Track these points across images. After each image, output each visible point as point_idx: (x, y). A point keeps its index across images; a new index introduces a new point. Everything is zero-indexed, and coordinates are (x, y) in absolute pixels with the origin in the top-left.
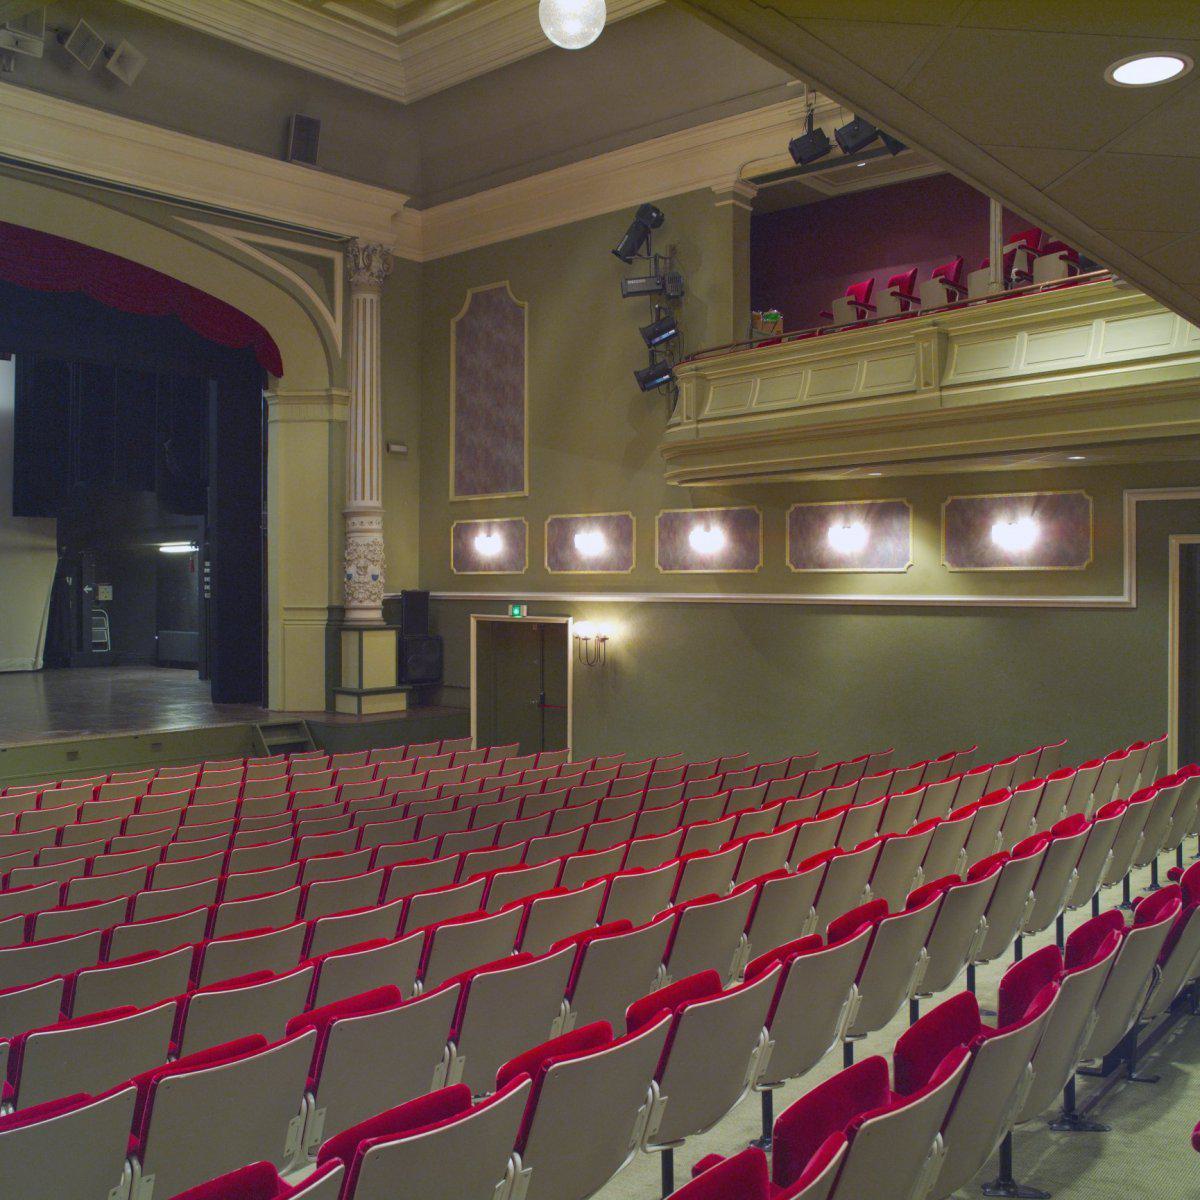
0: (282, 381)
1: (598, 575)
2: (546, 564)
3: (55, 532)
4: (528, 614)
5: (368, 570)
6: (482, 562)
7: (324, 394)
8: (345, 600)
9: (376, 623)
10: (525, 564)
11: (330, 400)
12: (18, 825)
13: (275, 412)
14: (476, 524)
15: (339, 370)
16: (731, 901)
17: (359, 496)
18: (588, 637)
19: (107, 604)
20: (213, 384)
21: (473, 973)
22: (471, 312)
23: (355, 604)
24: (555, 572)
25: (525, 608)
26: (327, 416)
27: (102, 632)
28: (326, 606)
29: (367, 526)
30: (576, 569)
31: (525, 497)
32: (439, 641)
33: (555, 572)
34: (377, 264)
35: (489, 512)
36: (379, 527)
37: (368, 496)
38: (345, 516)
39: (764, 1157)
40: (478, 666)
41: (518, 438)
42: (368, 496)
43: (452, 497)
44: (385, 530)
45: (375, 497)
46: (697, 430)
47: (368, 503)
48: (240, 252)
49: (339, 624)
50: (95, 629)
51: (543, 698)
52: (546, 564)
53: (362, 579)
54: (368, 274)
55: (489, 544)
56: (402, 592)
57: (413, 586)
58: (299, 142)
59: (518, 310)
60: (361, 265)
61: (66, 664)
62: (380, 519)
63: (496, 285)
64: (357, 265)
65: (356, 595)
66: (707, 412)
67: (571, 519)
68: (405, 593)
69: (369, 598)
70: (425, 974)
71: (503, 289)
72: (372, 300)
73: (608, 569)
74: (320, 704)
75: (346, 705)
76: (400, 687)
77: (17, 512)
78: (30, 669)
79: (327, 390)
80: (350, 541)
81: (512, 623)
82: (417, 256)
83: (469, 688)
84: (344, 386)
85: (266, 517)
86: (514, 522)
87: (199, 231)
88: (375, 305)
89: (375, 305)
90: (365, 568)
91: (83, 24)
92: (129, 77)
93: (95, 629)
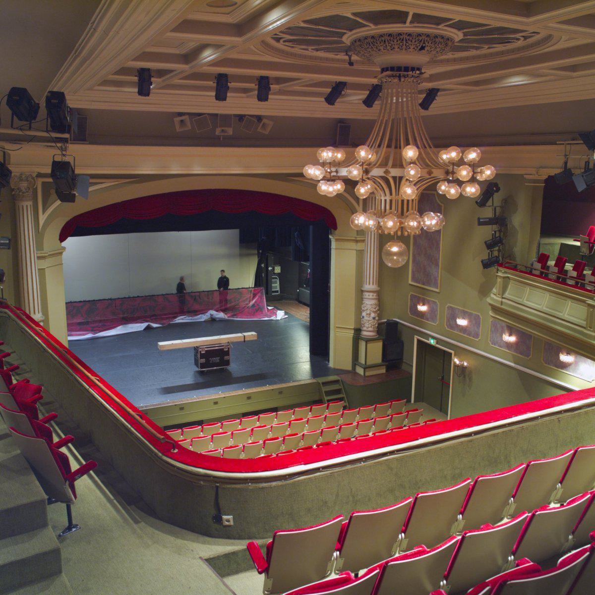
0: (337, 232)
13: (334, 245)
17: (368, 284)
19: (278, 274)
20: (311, 227)
27: (276, 286)
28: (353, 328)
32: (402, 343)
39: (441, 592)
41: (437, 265)
45: (375, 284)
46: (502, 302)
50: (273, 285)
66: (506, 295)
80: (364, 302)
93: (273, 285)
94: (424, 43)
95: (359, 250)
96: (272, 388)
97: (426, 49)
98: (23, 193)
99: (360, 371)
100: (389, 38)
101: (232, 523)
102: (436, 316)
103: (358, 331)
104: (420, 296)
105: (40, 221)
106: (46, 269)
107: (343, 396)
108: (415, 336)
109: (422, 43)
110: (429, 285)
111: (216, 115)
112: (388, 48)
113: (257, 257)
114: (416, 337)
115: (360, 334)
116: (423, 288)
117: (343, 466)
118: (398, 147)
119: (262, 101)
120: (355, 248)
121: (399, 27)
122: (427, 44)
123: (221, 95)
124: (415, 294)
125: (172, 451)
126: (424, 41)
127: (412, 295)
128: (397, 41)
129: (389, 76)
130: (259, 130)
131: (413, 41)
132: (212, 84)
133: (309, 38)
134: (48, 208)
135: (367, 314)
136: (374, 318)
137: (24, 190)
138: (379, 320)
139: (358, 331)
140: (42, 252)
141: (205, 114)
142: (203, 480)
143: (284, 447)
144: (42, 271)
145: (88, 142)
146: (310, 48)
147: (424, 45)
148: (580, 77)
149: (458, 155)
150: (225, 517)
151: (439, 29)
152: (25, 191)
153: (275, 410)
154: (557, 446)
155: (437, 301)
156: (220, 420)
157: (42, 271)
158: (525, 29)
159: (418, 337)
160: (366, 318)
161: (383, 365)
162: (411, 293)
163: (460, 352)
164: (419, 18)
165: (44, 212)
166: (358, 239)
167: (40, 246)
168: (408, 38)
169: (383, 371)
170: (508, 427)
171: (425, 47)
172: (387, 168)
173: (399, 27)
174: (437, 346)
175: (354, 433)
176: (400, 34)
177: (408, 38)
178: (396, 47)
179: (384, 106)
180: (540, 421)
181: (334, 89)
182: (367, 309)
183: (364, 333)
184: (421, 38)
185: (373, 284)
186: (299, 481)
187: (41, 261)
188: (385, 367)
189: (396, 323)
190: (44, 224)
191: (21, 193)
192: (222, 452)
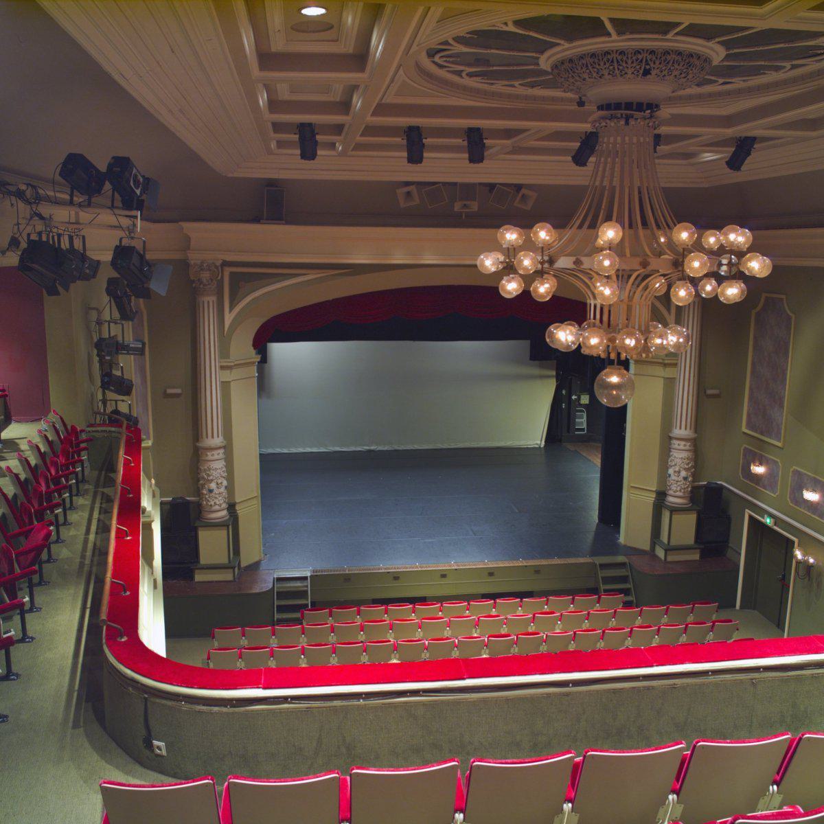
16: (281, 711)
17: (678, 427)
19: (585, 406)
28: (654, 489)
32: (729, 519)
41: (781, 406)
45: (683, 426)
59: (789, 318)
71: (782, 299)
76: (696, 546)
80: (671, 453)
94: (648, 64)
95: (668, 378)
96: (525, 564)
97: (653, 72)
99: (660, 553)
100: (592, 60)
101: (164, 752)
102: (776, 483)
103: (661, 495)
104: (756, 451)
105: (224, 331)
106: (232, 383)
107: (629, 586)
108: (747, 510)
109: (645, 64)
110: (770, 436)
111: (455, 184)
112: (595, 75)
113: (554, 380)
114: (748, 512)
115: (664, 500)
116: (761, 440)
117: (327, 700)
118: (594, 226)
119: (474, 163)
120: (663, 375)
121: (603, 43)
122: (652, 65)
123: (415, 156)
124: (750, 448)
125: (118, 640)
126: (646, 60)
127: (745, 449)
128: (605, 64)
129: (603, 118)
130: (517, 204)
131: (630, 62)
132: (399, 140)
133: (495, 68)
135: (675, 472)
136: (685, 479)
137: (205, 281)
138: (693, 481)
139: (661, 495)
140: (228, 360)
141: (439, 183)
142: (132, 686)
143: (602, 644)
144: (226, 386)
145: (284, 222)
146: (516, 83)
147: (648, 67)
148: (386, 92)
149: (691, 236)
150: (156, 743)
151: (667, 40)
153: (521, 595)
154: (751, 726)
155: (778, 460)
156: (441, 600)
157: (226, 386)
158: (748, 25)
159: (750, 512)
160: (673, 477)
161: (696, 548)
162: (745, 445)
163: (808, 542)
164: (623, 26)
165: (231, 309)
166: (666, 362)
167: (224, 352)
168: (619, 58)
169: (696, 556)
170: (642, 681)
171: (650, 70)
172: (579, 257)
173: (603, 43)
174: (775, 528)
175: (708, 638)
176: (607, 53)
177: (619, 58)
178: (606, 72)
179: (601, 165)
180: (711, 679)
181: (583, 143)
182: (676, 465)
183: (671, 500)
184: (640, 57)
185: (686, 429)
186: (252, 711)
187: (224, 372)
188: (699, 550)
189: (722, 487)
190: (229, 327)
191: (201, 286)
192: (545, 637)
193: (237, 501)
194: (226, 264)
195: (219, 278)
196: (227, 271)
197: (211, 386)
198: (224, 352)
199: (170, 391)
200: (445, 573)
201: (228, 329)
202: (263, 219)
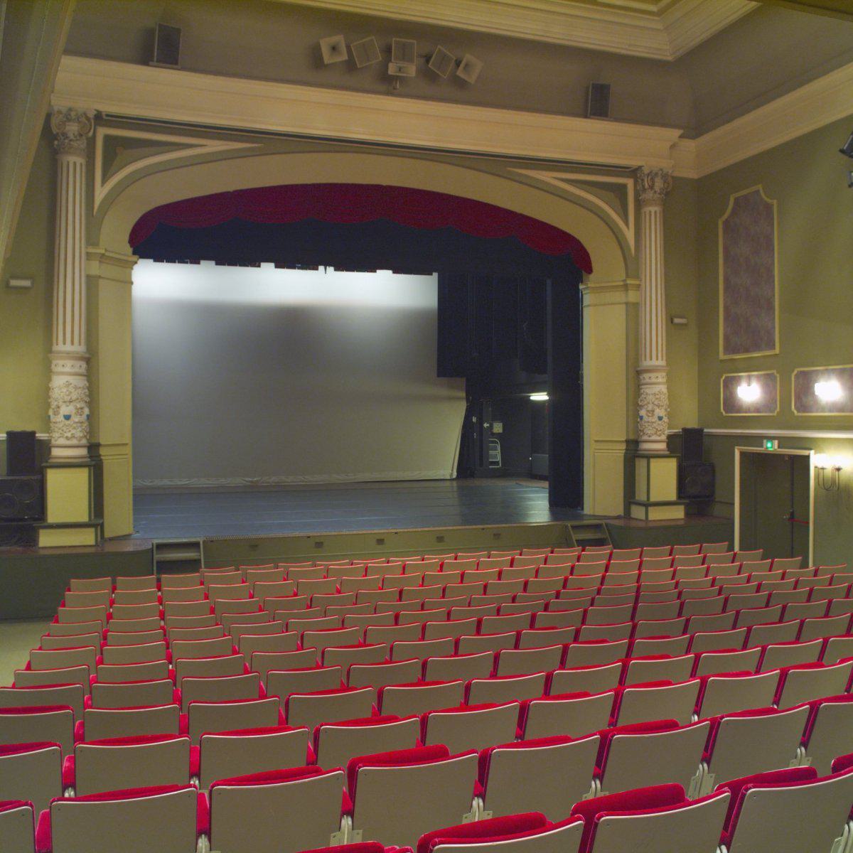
0: (592, 276)
1: (835, 417)
2: (793, 407)
3: (464, 387)
4: (779, 447)
5: (655, 413)
6: (744, 407)
7: (622, 283)
8: (639, 436)
9: (662, 453)
10: (776, 408)
11: (626, 287)
12: (105, 638)
13: (588, 299)
14: (739, 376)
15: (632, 265)
18: (825, 467)
20: (549, 282)
21: (820, 702)
22: (734, 212)
23: (645, 438)
24: (800, 414)
25: (776, 442)
26: (624, 299)
27: (496, 454)
29: (654, 380)
30: (817, 412)
31: (776, 355)
32: (713, 467)
33: (800, 414)
34: (659, 184)
35: (750, 367)
36: (664, 380)
37: (655, 358)
38: (639, 373)
40: (741, 486)
41: (770, 307)
42: (655, 358)
43: (722, 356)
44: (670, 382)
47: (654, 362)
48: (555, 186)
49: (634, 453)
50: (491, 452)
51: (792, 514)
52: (793, 407)
53: (650, 419)
54: (652, 192)
55: (749, 392)
56: (683, 429)
57: (692, 424)
58: (597, 103)
59: (769, 207)
60: (646, 186)
61: (472, 475)
62: (664, 374)
63: (753, 189)
64: (643, 186)
65: (647, 431)
67: (814, 371)
68: (685, 430)
69: (656, 433)
70: (779, 700)
72: (655, 212)
73: (843, 412)
74: (620, 511)
75: (638, 512)
76: (679, 501)
77: (440, 374)
78: (449, 478)
79: (624, 281)
80: (642, 391)
81: (766, 454)
82: (693, 175)
83: (733, 504)
84: (637, 277)
85: (582, 374)
86: (768, 375)
87: (532, 178)
88: (658, 215)
89: (658, 215)
90: (653, 411)
91: (439, 49)
92: (472, 79)
93: (491, 452)
98: (71, 140)
105: (98, 201)
108: (736, 447)
115: (638, 450)
134: (110, 177)
152: (75, 139)
165: (104, 182)
191: (66, 141)
193: (102, 442)
194: (100, 119)
195: (91, 134)
196: (102, 132)
197: (74, 273)
198: (92, 240)
199: (14, 283)
200: (382, 537)
201: (100, 206)
202: (153, 61)
